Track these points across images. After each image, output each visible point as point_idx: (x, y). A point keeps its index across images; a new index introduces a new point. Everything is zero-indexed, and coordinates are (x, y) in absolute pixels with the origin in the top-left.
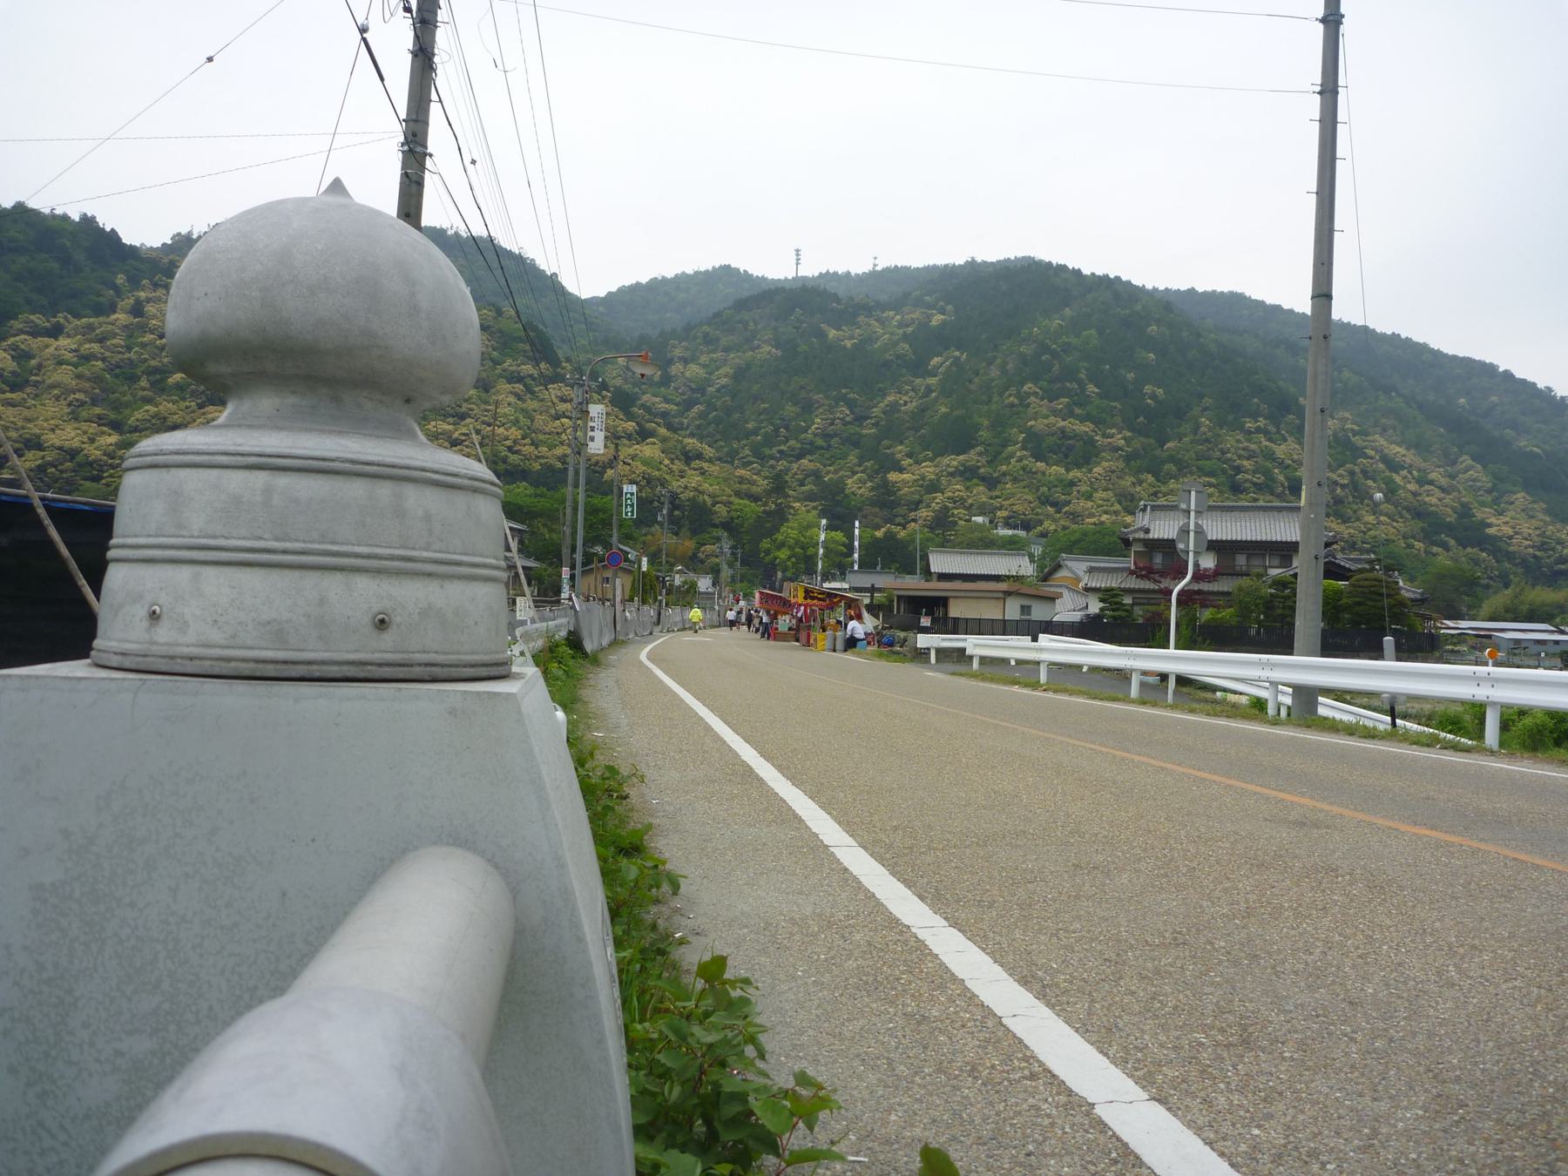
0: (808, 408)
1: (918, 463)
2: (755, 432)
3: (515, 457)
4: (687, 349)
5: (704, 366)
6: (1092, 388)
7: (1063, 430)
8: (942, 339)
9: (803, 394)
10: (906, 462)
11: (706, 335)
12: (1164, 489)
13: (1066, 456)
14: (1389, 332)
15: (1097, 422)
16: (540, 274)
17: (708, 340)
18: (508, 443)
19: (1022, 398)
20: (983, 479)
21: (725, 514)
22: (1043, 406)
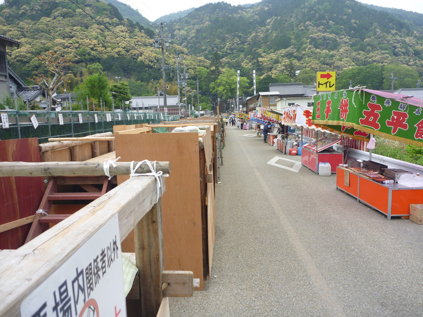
0: (224, 40)
1: (268, 54)
2: (205, 50)
3: (94, 52)
4: (180, 26)
5: (186, 31)
6: (331, 22)
7: (324, 37)
8: (270, 14)
9: (222, 35)
10: (263, 54)
11: (186, 20)
12: (369, 56)
13: (327, 47)
14: (409, 11)
15: (337, 34)
16: (132, 10)
17: (187, 22)
18: (91, 46)
19: (306, 27)
20: (296, 57)
21: (193, 73)
22: (315, 29)
